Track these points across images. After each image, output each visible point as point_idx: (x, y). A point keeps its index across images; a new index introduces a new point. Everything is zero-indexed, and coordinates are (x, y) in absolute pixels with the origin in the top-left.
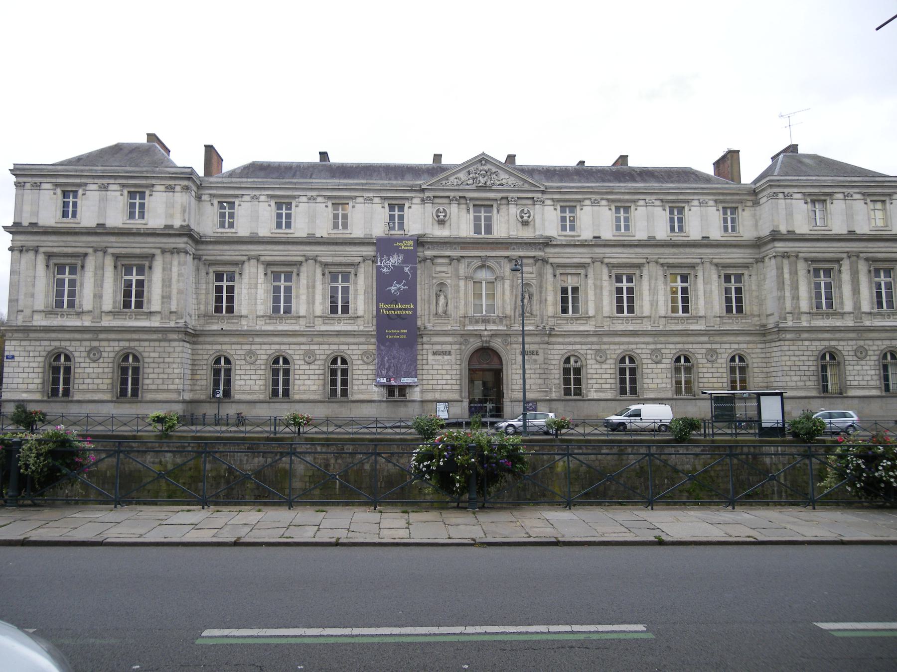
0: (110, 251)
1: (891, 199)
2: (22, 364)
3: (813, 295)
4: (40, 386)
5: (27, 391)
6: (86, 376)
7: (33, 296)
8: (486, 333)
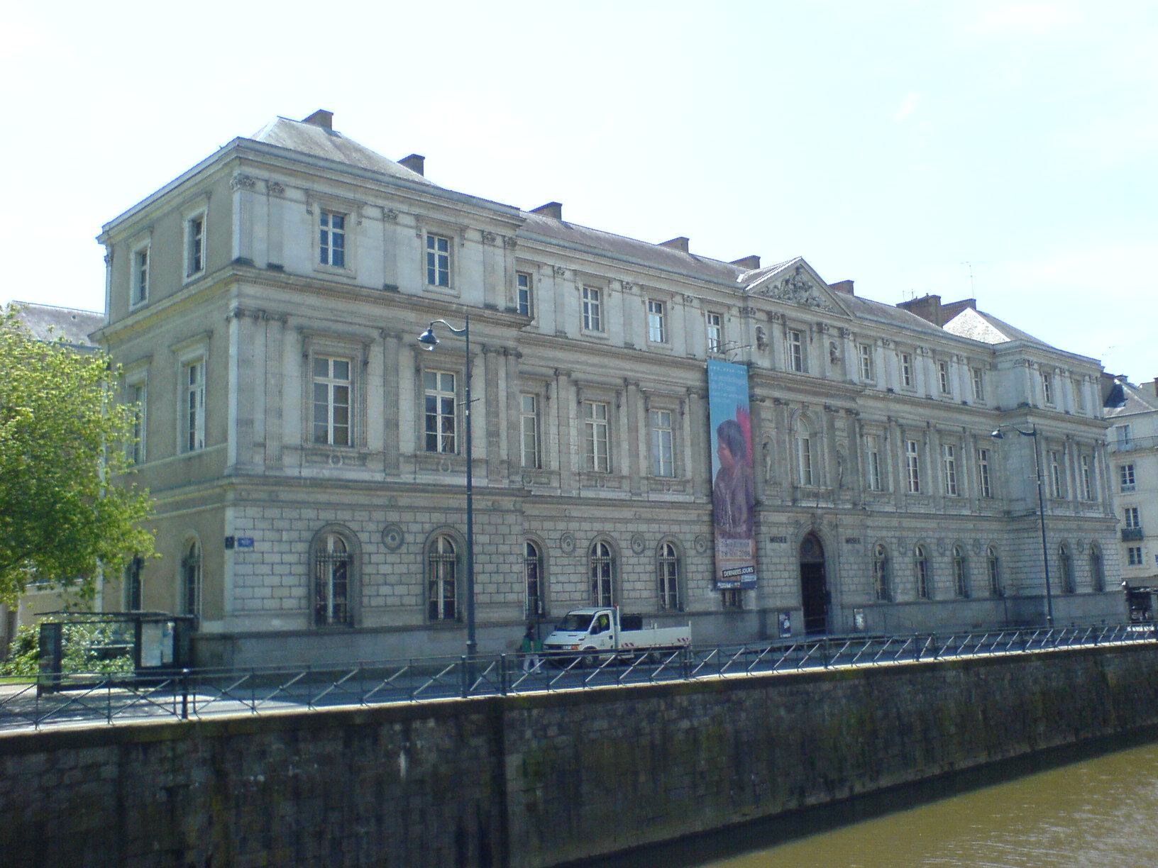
0: (292, 321)
1: (360, 215)
2: (268, 558)
3: (312, 412)
4: (304, 603)
5: (281, 613)
6: (380, 579)
7: (280, 414)
8: (819, 511)
